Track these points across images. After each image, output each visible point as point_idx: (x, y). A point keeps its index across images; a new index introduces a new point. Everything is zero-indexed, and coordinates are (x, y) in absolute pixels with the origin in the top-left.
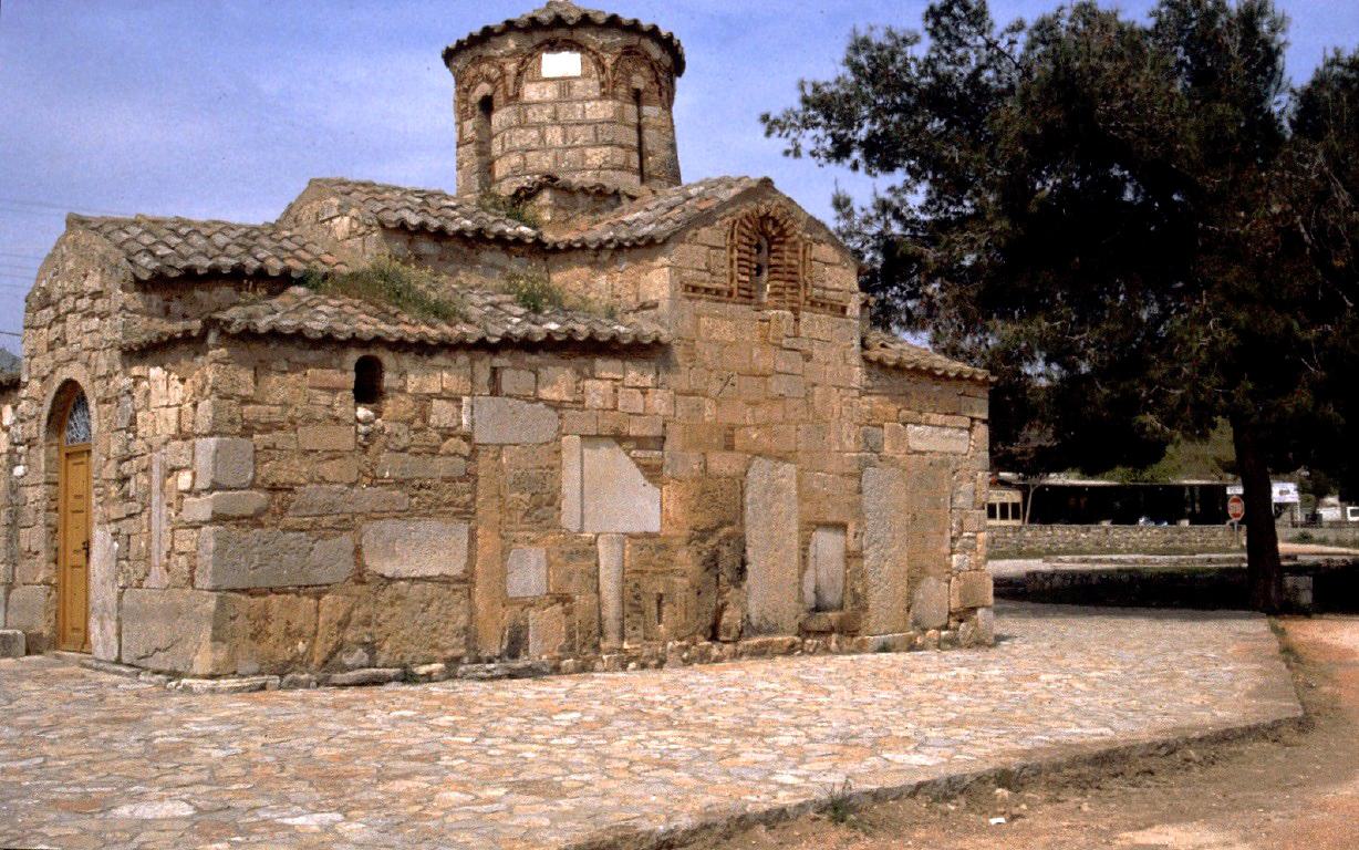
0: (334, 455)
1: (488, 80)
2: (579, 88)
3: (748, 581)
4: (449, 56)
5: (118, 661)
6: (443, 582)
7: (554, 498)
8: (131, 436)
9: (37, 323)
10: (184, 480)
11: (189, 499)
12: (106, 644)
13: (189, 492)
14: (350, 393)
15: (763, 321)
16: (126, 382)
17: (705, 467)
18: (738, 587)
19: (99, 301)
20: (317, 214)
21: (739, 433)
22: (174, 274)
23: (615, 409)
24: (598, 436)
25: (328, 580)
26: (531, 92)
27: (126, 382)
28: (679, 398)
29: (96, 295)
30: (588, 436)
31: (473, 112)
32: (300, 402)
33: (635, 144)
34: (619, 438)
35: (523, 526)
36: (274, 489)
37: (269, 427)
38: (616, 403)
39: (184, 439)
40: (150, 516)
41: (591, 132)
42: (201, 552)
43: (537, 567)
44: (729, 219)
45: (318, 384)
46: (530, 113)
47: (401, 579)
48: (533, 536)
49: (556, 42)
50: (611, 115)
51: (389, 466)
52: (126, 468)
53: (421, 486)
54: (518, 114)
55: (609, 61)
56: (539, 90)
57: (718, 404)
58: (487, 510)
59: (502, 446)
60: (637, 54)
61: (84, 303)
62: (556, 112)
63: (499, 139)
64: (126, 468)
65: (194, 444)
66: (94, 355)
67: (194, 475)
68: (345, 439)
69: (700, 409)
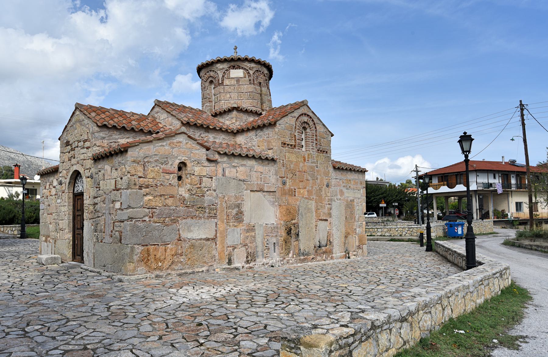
4: (78, 107)
8: (98, 189)
9: (65, 152)
11: (119, 212)
12: (89, 261)
13: (119, 209)
19: (86, 143)
26: (226, 82)
29: (85, 141)
39: (117, 190)
48: (236, 224)
52: (96, 200)
55: (251, 72)
61: (81, 144)
64: (96, 200)
66: (84, 161)
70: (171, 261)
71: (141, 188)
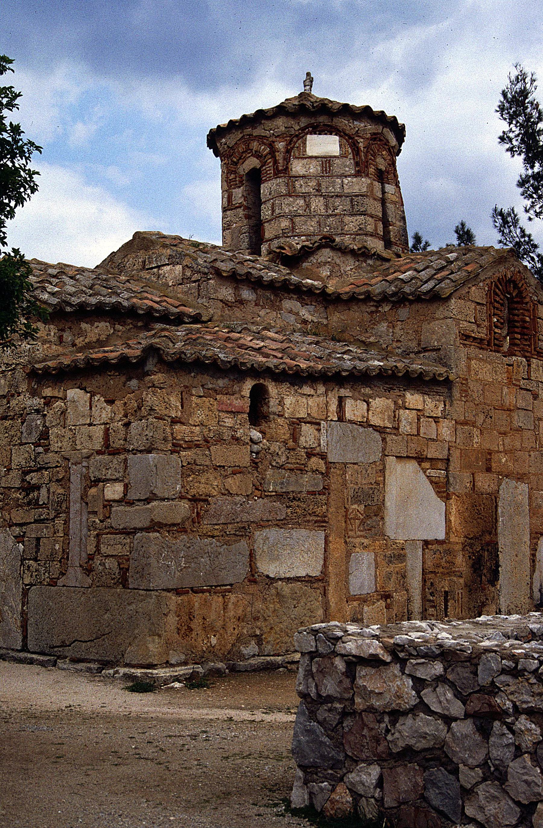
0: (237, 471)
1: (257, 155)
2: (337, 167)
3: (499, 581)
5: (25, 648)
6: (307, 581)
7: (380, 509)
8: (41, 449)
10: (114, 491)
14: (246, 416)
15: (509, 365)
16: (37, 402)
17: (474, 485)
18: (494, 585)
20: (144, 262)
21: (495, 457)
22: (68, 309)
23: (418, 434)
24: (408, 457)
25: (231, 580)
26: (298, 167)
27: (37, 402)
28: (459, 427)
30: (401, 457)
31: (241, 182)
32: (213, 424)
33: (380, 215)
34: (420, 459)
35: (359, 533)
36: (194, 500)
37: (191, 445)
38: (418, 431)
40: (66, 522)
41: (348, 203)
42: (135, 555)
43: (369, 568)
44: (488, 281)
45: (224, 408)
46: (297, 184)
47: (280, 579)
49: (318, 126)
50: (365, 190)
51: (273, 481)
53: (294, 498)
54: (287, 185)
56: (304, 166)
57: (481, 433)
58: (336, 519)
59: (345, 464)
60: (380, 140)
62: (319, 185)
63: (269, 205)
64: (33, 478)
65: (126, 460)
67: (126, 486)
68: (242, 456)
69: (471, 436)
70: (236, 632)
71: (176, 448)
